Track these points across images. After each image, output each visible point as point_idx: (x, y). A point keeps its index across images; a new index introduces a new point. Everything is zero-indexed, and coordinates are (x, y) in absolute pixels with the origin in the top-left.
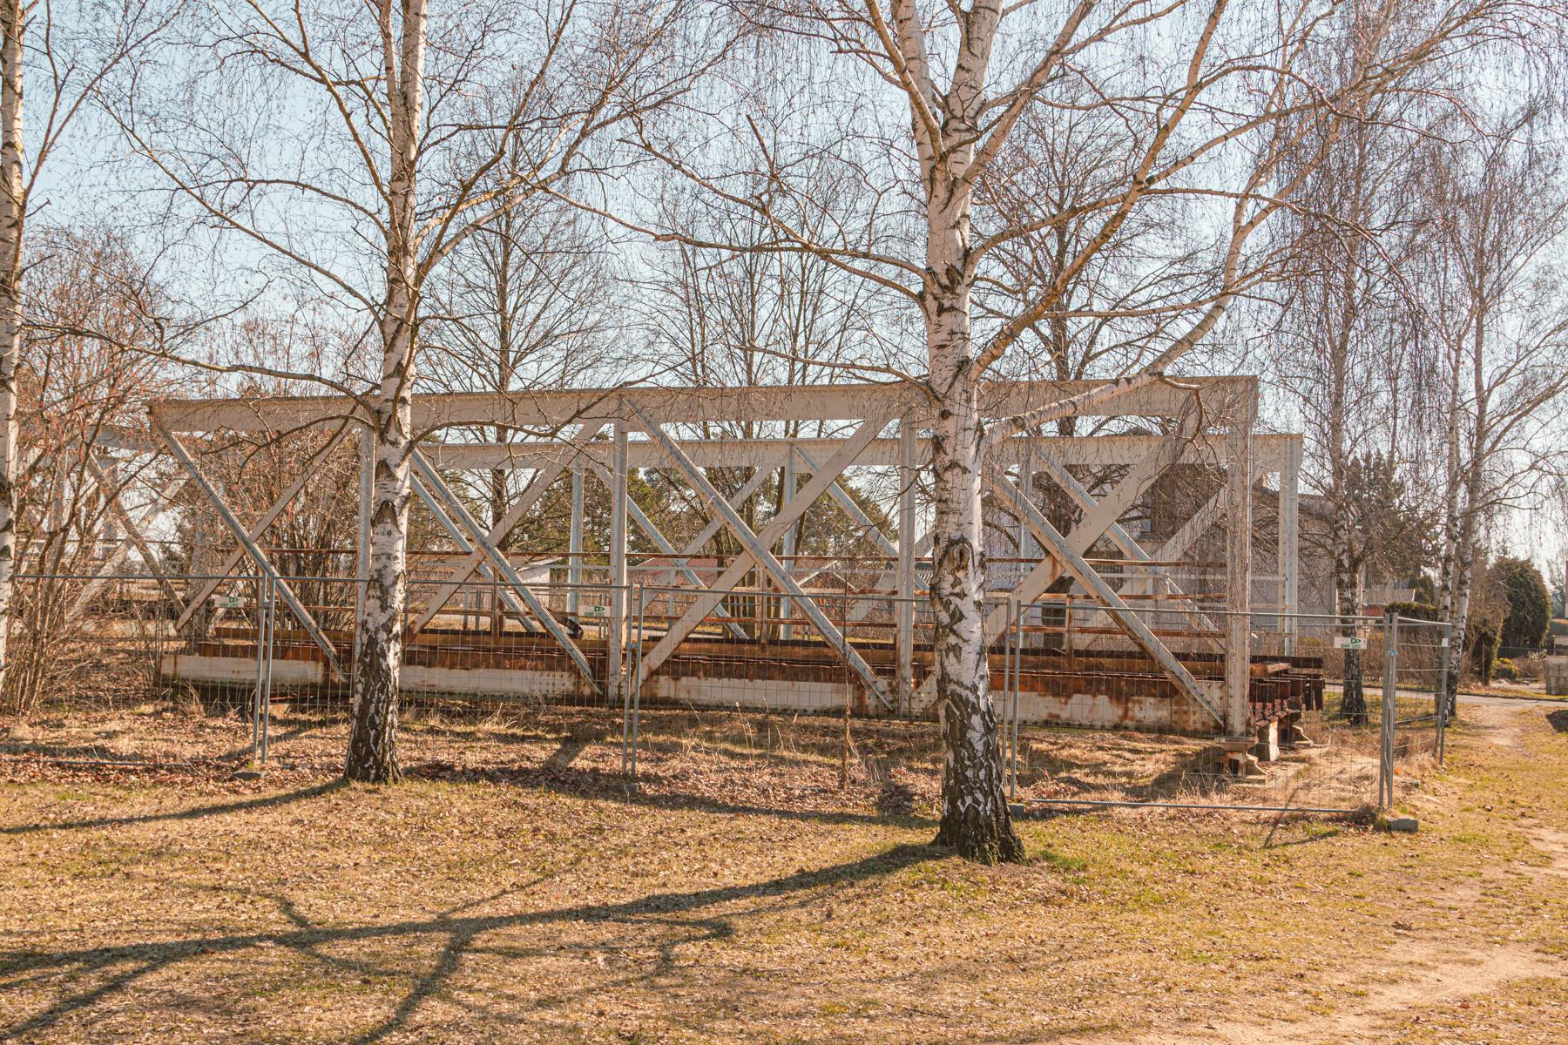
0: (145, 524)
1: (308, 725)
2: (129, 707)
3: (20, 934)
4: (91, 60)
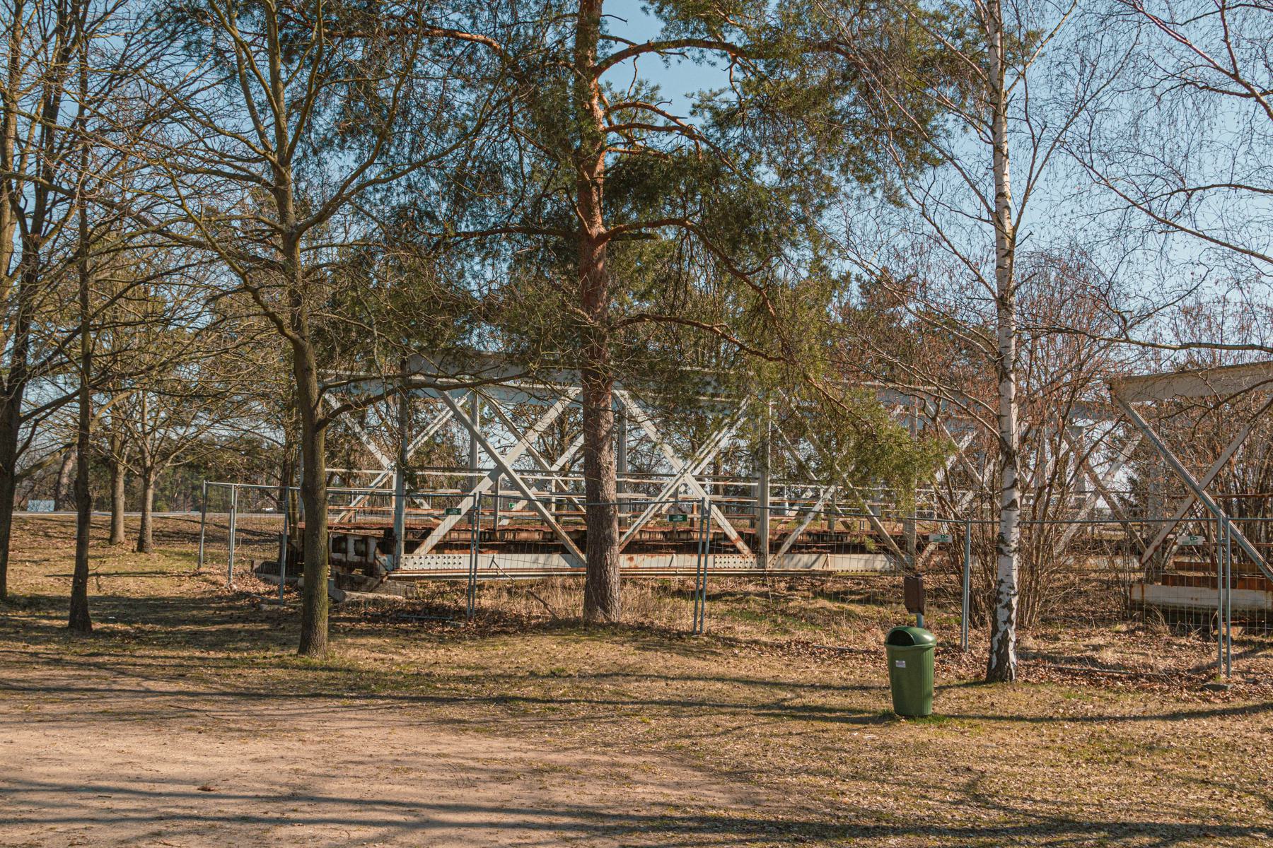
0: (1109, 478)
1: (1262, 646)
2: (1107, 626)
3: (1054, 803)
4: (1058, 118)
